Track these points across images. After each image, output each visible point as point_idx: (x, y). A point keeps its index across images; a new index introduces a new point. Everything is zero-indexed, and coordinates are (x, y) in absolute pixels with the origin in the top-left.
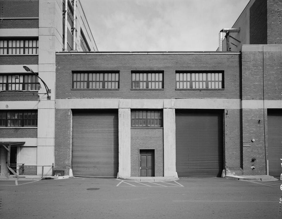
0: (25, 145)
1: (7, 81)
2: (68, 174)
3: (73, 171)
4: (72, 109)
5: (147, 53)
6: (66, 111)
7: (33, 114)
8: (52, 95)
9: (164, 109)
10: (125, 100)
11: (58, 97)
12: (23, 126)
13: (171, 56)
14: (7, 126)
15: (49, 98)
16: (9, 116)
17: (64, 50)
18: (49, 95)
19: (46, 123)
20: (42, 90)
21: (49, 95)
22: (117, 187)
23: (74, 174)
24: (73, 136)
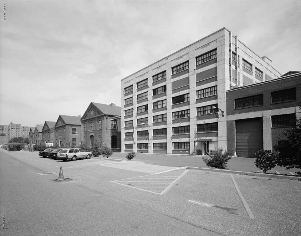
0: (212, 140)
1: (204, 110)
2: (234, 155)
3: (237, 154)
4: (235, 120)
5: (282, 79)
6: (232, 121)
7: (216, 124)
8: (225, 114)
9: (296, 114)
10: (267, 111)
11: (227, 115)
12: (211, 131)
13: (235, 92)
14: (204, 131)
15: (223, 116)
16: (205, 126)
17: (74, 130)
18: (223, 114)
19: (222, 129)
20: (220, 112)
21: (223, 114)
22: (293, 157)
23: (237, 155)
24: (119, 164)
